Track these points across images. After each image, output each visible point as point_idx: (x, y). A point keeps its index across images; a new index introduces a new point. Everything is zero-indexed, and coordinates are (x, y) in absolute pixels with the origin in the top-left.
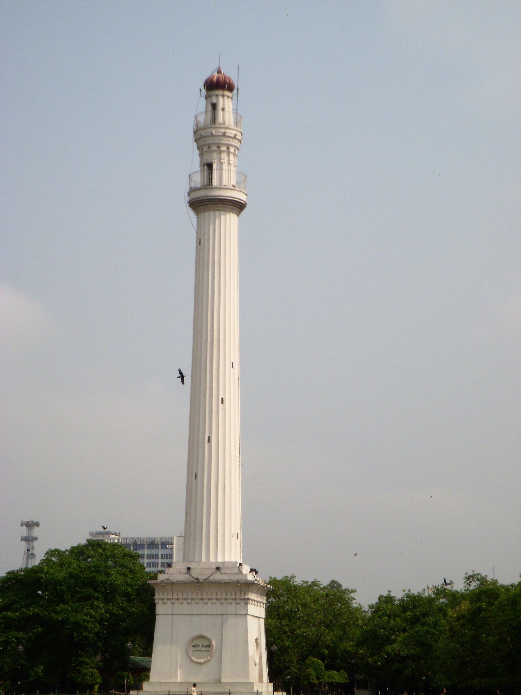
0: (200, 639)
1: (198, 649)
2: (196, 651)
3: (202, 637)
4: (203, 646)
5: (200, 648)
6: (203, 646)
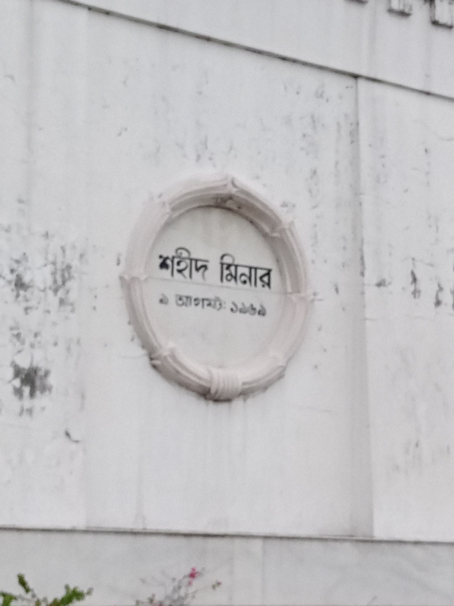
0: (216, 216)
1: (194, 285)
2: (184, 300)
3: (230, 204)
4: (229, 271)
5: (209, 283)
6: (229, 271)
